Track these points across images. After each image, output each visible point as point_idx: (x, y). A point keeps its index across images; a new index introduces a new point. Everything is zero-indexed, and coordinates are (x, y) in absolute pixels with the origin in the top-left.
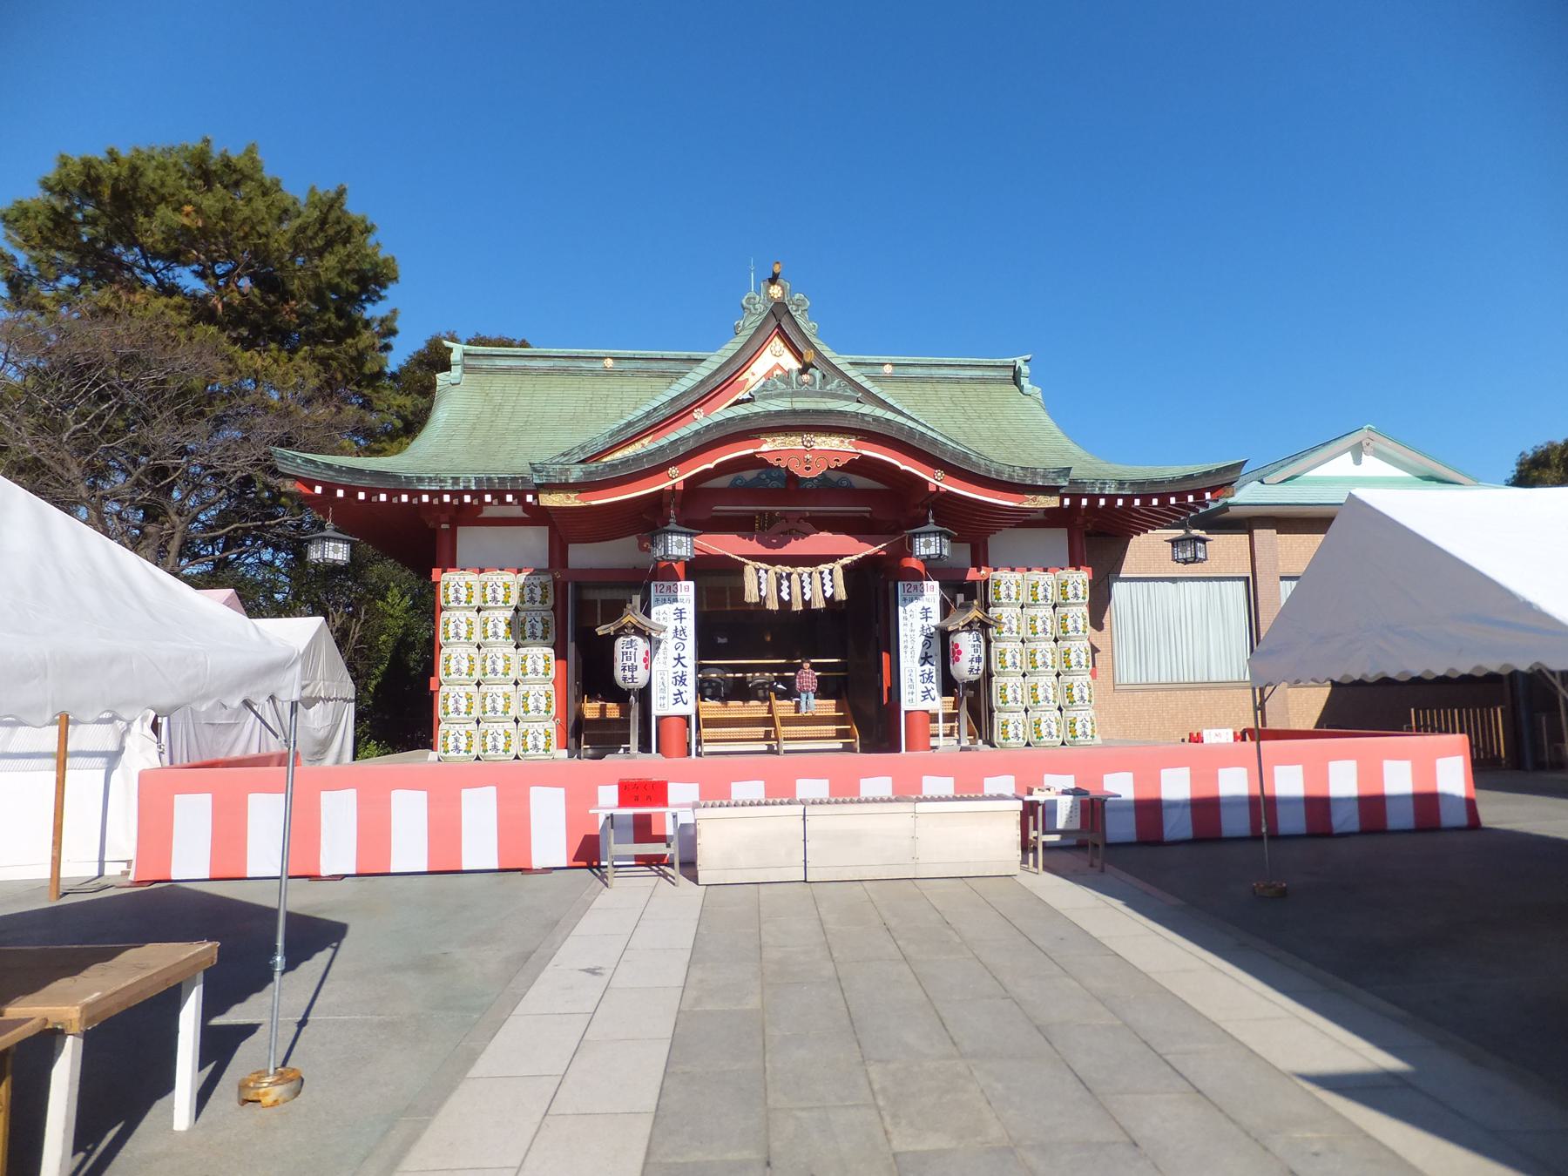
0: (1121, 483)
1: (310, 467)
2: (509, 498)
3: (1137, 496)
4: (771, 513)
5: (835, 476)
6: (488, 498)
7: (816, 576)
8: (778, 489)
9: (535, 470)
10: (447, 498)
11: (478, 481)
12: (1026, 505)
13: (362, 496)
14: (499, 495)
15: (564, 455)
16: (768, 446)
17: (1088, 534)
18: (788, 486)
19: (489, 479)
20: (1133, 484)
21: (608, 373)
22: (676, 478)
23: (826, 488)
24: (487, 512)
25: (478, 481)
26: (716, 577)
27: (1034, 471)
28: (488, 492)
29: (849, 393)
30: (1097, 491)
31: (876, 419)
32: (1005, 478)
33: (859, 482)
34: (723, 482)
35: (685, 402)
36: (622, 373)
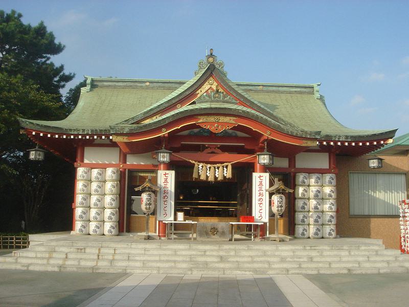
0: (347, 137)
1: (31, 125)
2: (103, 137)
3: (353, 142)
4: (204, 145)
5: (231, 131)
6: (95, 137)
7: (212, 168)
8: (207, 136)
9: (111, 128)
10: (80, 137)
11: (92, 131)
12: (303, 145)
13: (49, 136)
14: (100, 136)
15: (126, 121)
16: (201, 120)
17: (337, 155)
18: (212, 136)
19: (96, 130)
20: (352, 137)
21: (147, 88)
22: (165, 133)
23: (225, 136)
24: (96, 142)
25: (92, 131)
26: (183, 171)
27: (306, 133)
28: (96, 135)
29: (234, 101)
30: (337, 139)
31: (243, 111)
32: (295, 134)
33: (240, 134)
34: (186, 132)
35: (174, 102)
36: (153, 88)
